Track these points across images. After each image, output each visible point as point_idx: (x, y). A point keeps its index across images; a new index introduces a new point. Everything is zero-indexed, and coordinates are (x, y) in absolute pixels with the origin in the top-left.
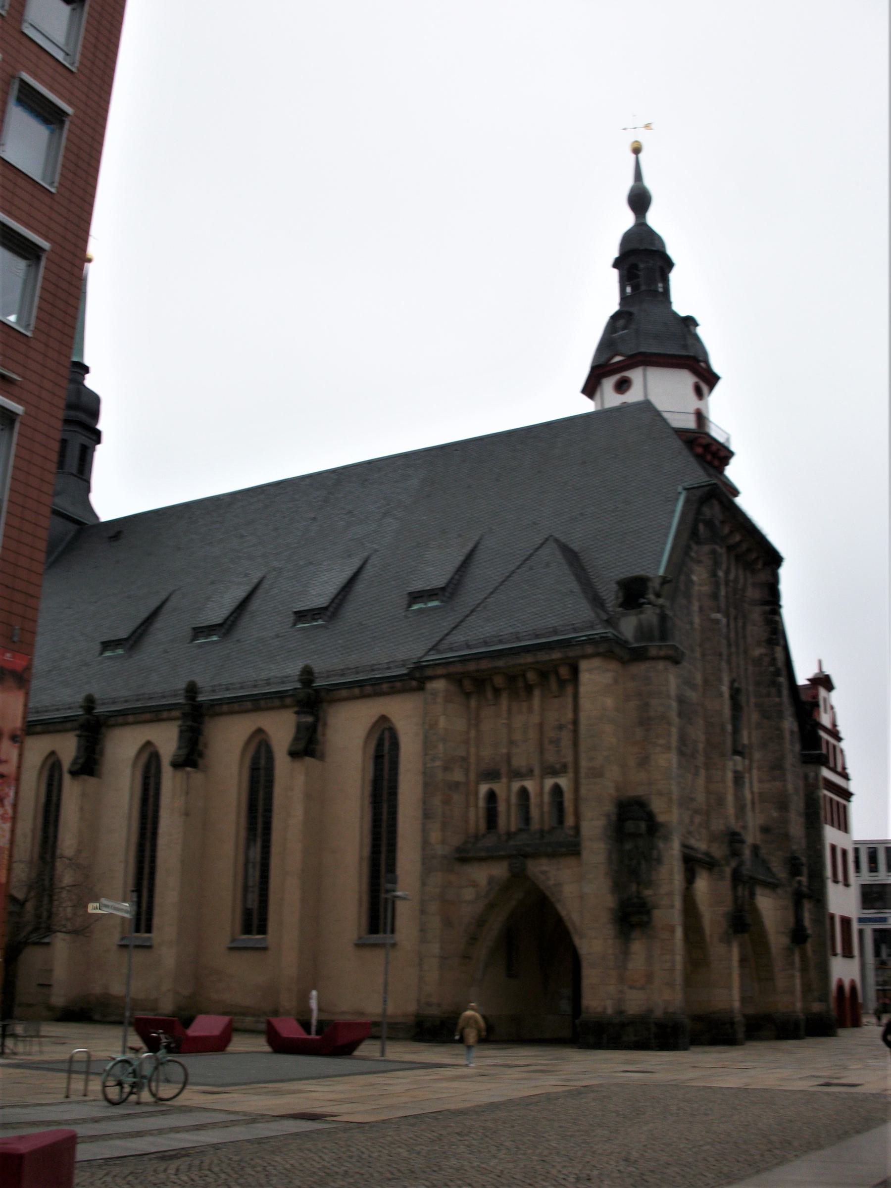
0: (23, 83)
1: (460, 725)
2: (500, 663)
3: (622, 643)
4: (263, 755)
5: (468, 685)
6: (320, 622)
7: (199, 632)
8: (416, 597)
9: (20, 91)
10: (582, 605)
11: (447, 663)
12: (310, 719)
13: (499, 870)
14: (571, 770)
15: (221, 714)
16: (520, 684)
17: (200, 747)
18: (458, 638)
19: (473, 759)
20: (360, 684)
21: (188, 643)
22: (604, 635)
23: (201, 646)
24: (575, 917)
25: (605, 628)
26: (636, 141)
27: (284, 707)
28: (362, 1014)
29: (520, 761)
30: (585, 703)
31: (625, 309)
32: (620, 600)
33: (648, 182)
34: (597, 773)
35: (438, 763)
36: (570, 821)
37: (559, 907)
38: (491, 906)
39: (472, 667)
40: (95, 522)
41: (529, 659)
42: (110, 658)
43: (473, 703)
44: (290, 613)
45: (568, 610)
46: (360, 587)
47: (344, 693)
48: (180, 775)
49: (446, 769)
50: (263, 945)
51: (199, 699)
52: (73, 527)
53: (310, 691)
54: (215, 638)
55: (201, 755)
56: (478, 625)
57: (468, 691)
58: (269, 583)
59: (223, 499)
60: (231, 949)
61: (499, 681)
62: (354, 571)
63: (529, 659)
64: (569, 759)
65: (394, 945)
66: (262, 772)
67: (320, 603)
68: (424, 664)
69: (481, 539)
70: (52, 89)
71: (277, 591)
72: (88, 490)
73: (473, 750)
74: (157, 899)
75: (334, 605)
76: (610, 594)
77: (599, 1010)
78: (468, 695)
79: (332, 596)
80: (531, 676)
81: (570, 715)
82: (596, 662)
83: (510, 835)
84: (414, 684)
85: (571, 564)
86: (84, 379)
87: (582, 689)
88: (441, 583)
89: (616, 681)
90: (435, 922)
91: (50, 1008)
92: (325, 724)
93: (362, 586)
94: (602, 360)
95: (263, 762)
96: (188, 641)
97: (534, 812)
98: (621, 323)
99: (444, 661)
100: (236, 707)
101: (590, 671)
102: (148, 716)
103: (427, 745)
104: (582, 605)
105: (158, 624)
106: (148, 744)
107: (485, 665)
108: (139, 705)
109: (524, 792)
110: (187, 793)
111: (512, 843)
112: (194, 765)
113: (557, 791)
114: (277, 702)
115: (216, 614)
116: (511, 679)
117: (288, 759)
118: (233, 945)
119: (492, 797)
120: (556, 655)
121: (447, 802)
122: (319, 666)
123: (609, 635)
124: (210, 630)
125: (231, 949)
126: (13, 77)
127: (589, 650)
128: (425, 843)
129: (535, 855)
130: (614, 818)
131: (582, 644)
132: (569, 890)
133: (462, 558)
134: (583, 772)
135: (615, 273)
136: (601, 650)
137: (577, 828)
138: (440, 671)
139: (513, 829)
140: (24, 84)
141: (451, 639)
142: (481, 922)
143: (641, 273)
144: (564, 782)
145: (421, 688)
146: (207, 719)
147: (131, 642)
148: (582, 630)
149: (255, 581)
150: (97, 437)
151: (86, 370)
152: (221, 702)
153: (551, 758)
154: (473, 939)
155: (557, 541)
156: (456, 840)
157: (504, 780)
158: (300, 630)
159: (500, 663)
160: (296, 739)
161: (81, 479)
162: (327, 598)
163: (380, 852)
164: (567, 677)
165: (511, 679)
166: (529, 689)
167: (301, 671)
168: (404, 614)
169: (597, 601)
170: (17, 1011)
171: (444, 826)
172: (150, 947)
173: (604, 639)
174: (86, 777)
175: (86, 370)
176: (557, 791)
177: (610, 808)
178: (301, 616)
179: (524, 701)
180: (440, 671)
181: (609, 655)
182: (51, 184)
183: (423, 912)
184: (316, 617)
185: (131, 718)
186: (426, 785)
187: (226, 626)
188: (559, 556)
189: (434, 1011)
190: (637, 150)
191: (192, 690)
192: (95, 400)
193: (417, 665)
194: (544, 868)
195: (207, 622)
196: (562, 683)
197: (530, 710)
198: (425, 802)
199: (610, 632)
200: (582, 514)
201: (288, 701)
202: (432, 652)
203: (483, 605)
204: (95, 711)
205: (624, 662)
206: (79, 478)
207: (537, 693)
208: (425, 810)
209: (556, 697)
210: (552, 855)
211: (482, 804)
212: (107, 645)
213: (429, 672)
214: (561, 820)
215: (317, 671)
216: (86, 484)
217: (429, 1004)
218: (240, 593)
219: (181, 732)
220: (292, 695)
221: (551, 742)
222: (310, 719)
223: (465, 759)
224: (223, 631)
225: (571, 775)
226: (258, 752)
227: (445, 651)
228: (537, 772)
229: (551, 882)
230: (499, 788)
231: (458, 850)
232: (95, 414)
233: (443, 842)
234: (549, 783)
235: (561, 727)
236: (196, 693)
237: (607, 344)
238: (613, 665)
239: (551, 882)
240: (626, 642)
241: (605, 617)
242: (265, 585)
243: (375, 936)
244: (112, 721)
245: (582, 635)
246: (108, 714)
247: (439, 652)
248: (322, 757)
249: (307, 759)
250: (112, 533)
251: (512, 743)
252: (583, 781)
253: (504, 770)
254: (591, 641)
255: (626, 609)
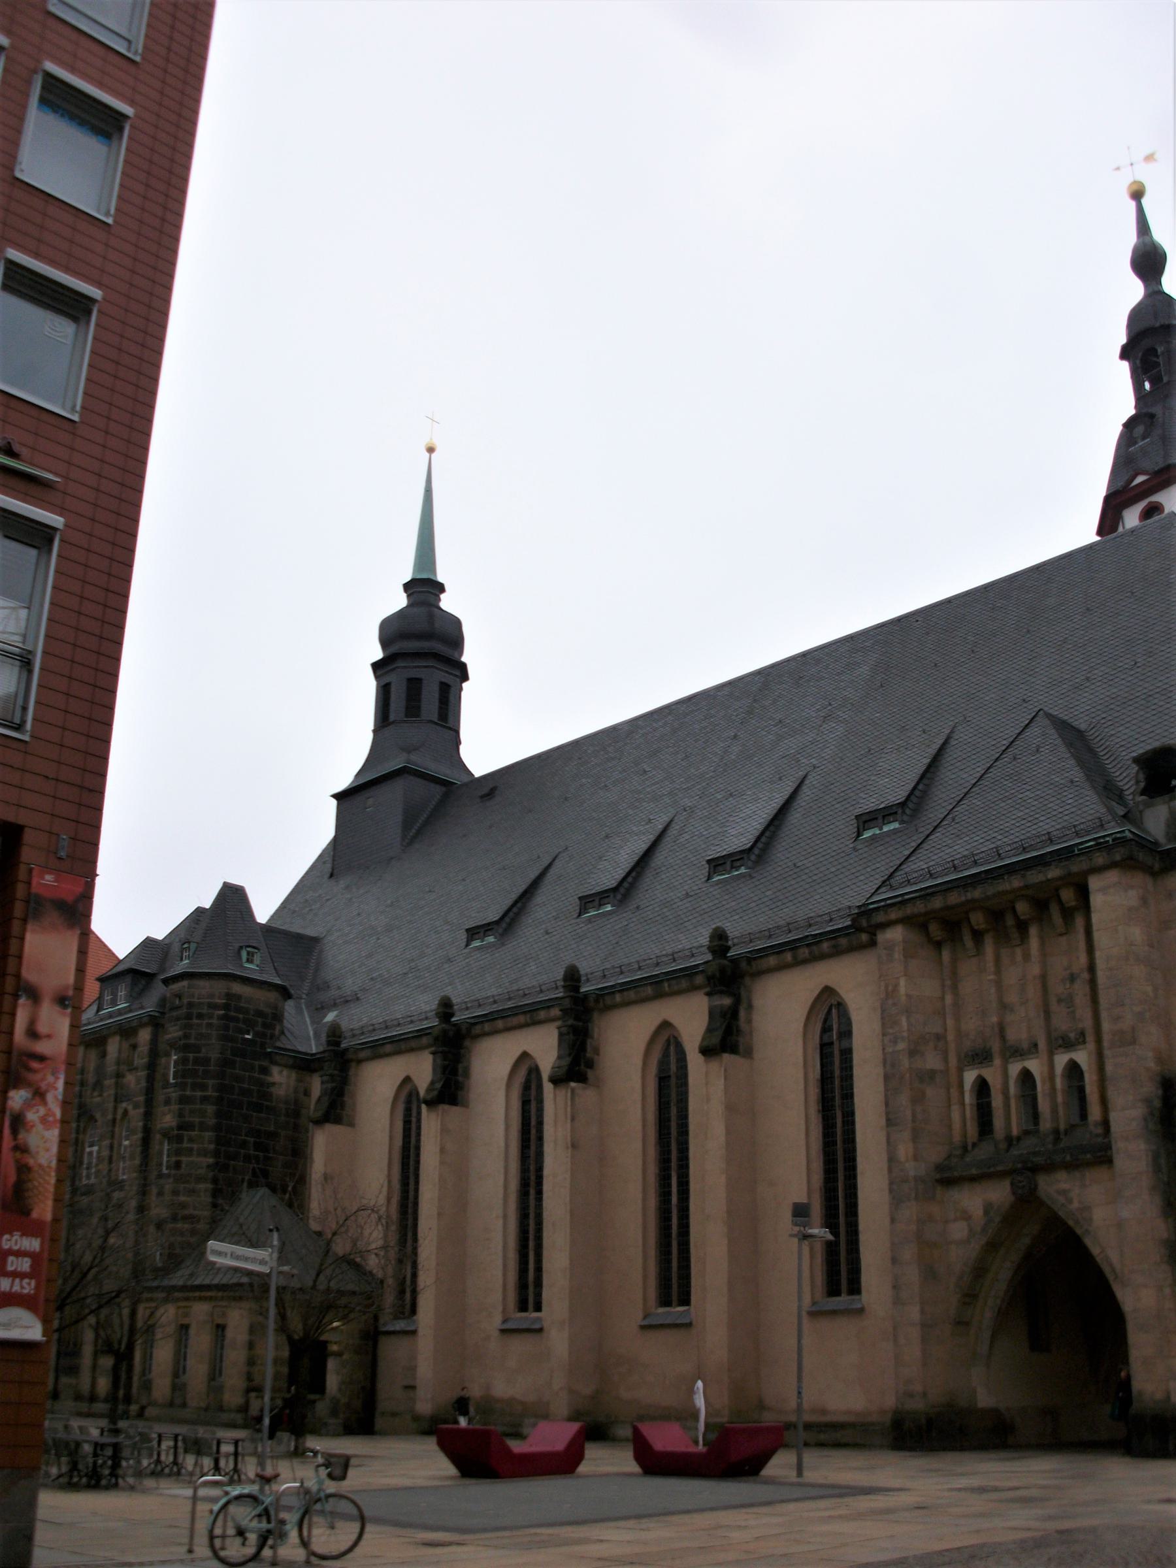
0: (48, 76)
1: (928, 988)
2: (977, 893)
3: (1150, 846)
4: (673, 1059)
5: (935, 929)
6: (743, 870)
7: (587, 902)
8: (867, 820)
9: (43, 88)
10: (1088, 798)
11: (903, 902)
12: (727, 1001)
13: (999, 1193)
14: (1090, 1038)
15: (615, 1006)
16: (1010, 921)
17: (589, 1054)
18: (918, 864)
19: (951, 1037)
20: (792, 946)
21: (574, 919)
22: (1118, 835)
23: (590, 920)
24: (1114, 1256)
25: (1119, 825)
26: (1135, 182)
27: (694, 988)
28: (824, 1411)
29: (1017, 1034)
30: (1101, 938)
31: (1145, 410)
32: (1142, 785)
33: (1160, 235)
34: (1128, 1039)
35: (901, 1046)
36: (1095, 1113)
37: (1088, 1241)
38: (992, 1247)
39: (937, 903)
40: (466, 779)
41: (1016, 882)
42: (478, 948)
43: (946, 955)
44: (704, 863)
45: (1068, 807)
46: (795, 817)
47: (772, 961)
48: (563, 1093)
49: (913, 1053)
50: (687, 1321)
51: (582, 990)
52: (438, 790)
53: (725, 962)
54: (609, 908)
55: (590, 1064)
56: (944, 844)
57: (939, 938)
58: (678, 827)
59: (621, 729)
60: (643, 1328)
61: (978, 919)
62: (786, 797)
63: (1016, 882)
64: (1088, 1024)
65: (861, 1311)
66: (673, 1080)
67: (741, 844)
68: (872, 906)
69: (952, 732)
70: (100, 85)
71: (687, 838)
72: (458, 742)
73: (950, 1022)
74: (546, 1265)
75: (760, 845)
76: (1128, 778)
77: (1159, 1396)
78: (938, 945)
79: (757, 833)
80: (1022, 908)
81: (1083, 959)
82: (1112, 876)
83: (1010, 1141)
84: (864, 937)
85: (1070, 745)
86: (440, 600)
87: (1095, 918)
88: (900, 797)
89: (1144, 901)
90: (912, 1275)
91: (416, 1418)
92: (750, 1007)
93: (798, 815)
94: (1120, 484)
95: (673, 1067)
96: (575, 916)
97: (1044, 1105)
98: (1139, 430)
99: (899, 899)
100: (632, 995)
101: (1103, 890)
102: (521, 1019)
103: (887, 1021)
104: (1088, 798)
105: (540, 898)
106: (525, 1055)
107: (954, 898)
108: (510, 1004)
109: (1027, 1077)
110: (573, 1119)
111: (1015, 1152)
112: (582, 1078)
113: (1074, 1069)
114: (684, 984)
115: (608, 876)
116: (996, 916)
117: (701, 1058)
118: (646, 1323)
119: (982, 1087)
120: (1053, 873)
121: (918, 1099)
122: (735, 928)
123: (1127, 834)
124: (601, 897)
125: (643, 1328)
126: (35, 72)
127: (1100, 859)
128: (892, 1159)
129: (1049, 1168)
130: (1157, 1103)
131: (1087, 852)
132: (1100, 1216)
133: (927, 761)
134: (1106, 1038)
135: (1125, 366)
136: (1118, 857)
137: (1106, 1123)
138: (893, 915)
139: (1015, 1132)
140: (50, 80)
141: (906, 868)
142: (979, 1271)
143: (1161, 360)
144: (1082, 1057)
145: (873, 943)
146: (596, 1015)
147: (504, 925)
148: (1088, 833)
149: (660, 827)
150: (463, 674)
151: (441, 588)
152: (612, 991)
153: (1061, 1023)
154: (970, 1297)
155: (1048, 716)
156: (935, 1154)
157: (997, 1062)
158: (717, 884)
159: (977, 893)
160: (709, 1030)
161: (445, 727)
162: (750, 837)
163: (836, 1180)
164: (1073, 903)
165: (996, 916)
166: (1022, 927)
167: (710, 937)
168: (851, 846)
169: (1109, 790)
170: (379, 1423)
171: (915, 1137)
172: (540, 1330)
173: (1120, 842)
174: (446, 1107)
175: (441, 588)
176: (1074, 1069)
177: (1150, 1089)
178: (716, 865)
179: (1016, 946)
180: (893, 915)
181: (1128, 864)
182: (107, 214)
183: (894, 1260)
184: (738, 864)
185: (500, 1024)
186: (887, 1078)
187: (622, 890)
188: (1052, 733)
189: (917, 1405)
190: (1137, 195)
191: (572, 978)
192: (456, 623)
193: (863, 909)
194: (1064, 1186)
195: (599, 888)
196: (1068, 914)
197: (1027, 957)
198: (887, 1104)
199: (1127, 830)
200: (1088, 679)
201: (699, 980)
202: (883, 889)
203: (950, 816)
204: (453, 1019)
205: (1154, 874)
206: (441, 726)
207: (1033, 931)
208: (887, 1114)
209: (1061, 935)
210: (1073, 1166)
211: (968, 1098)
212: (473, 933)
213: (880, 918)
214: (1084, 1115)
215: (737, 934)
216: (454, 734)
217: (910, 1395)
218: (640, 845)
219: (561, 1035)
220: (702, 971)
221: (1060, 1001)
222: (727, 1001)
223: (940, 1037)
224: (619, 897)
225: (1091, 1045)
226: (666, 1054)
227: (901, 885)
228: (1042, 1045)
229: (1076, 1205)
230: (992, 1075)
231: (939, 1168)
232: (457, 641)
233: (916, 1158)
234: (1061, 1060)
235: (1072, 978)
236: (578, 980)
237: (1125, 460)
238: (1139, 879)
239: (1076, 1205)
240: (1156, 843)
241: (1121, 811)
242: (673, 832)
243: (834, 1299)
244: (477, 1030)
245: (1088, 840)
246: (472, 1021)
247: (892, 888)
248: (748, 1053)
249: (726, 1056)
250: (486, 790)
251: (1004, 1007)
252: (1107, 1052)
253: (996, 1047)
254: (1101, 846)
255: (1151, 797)
